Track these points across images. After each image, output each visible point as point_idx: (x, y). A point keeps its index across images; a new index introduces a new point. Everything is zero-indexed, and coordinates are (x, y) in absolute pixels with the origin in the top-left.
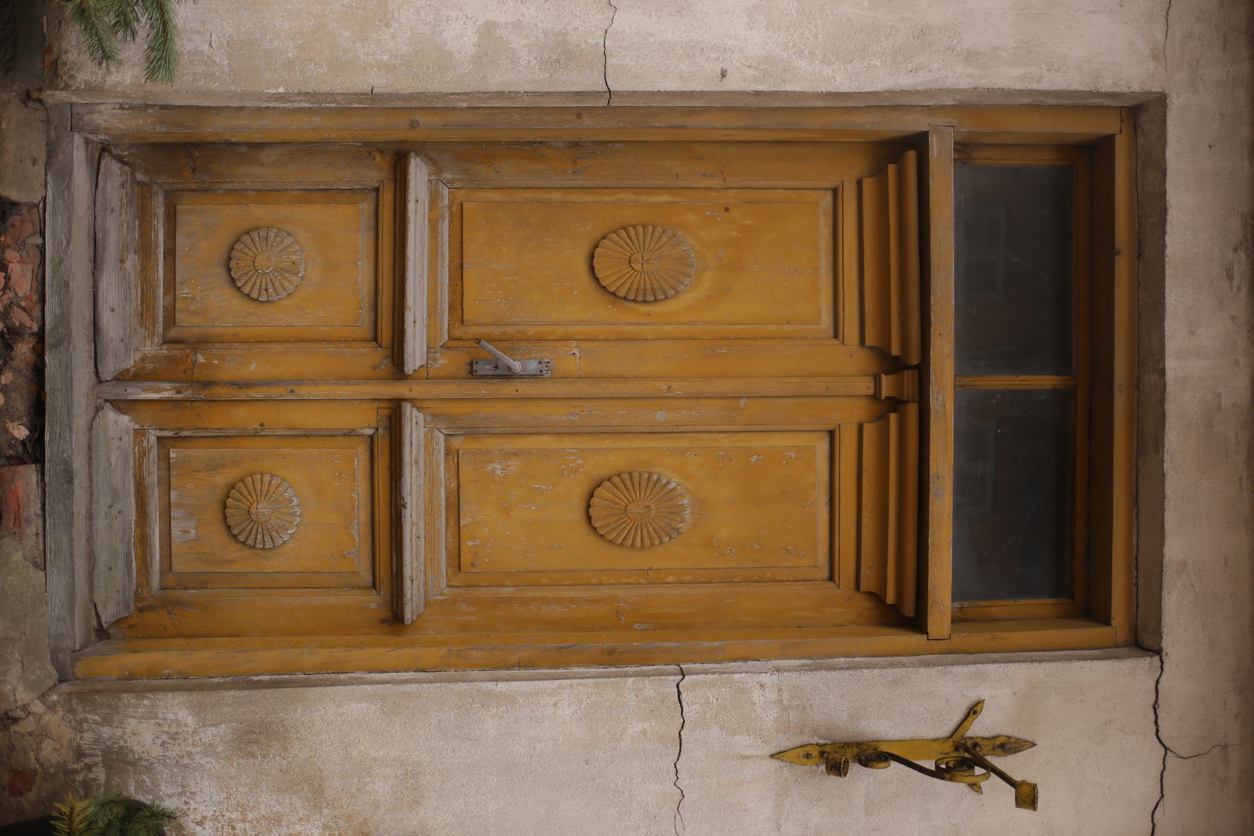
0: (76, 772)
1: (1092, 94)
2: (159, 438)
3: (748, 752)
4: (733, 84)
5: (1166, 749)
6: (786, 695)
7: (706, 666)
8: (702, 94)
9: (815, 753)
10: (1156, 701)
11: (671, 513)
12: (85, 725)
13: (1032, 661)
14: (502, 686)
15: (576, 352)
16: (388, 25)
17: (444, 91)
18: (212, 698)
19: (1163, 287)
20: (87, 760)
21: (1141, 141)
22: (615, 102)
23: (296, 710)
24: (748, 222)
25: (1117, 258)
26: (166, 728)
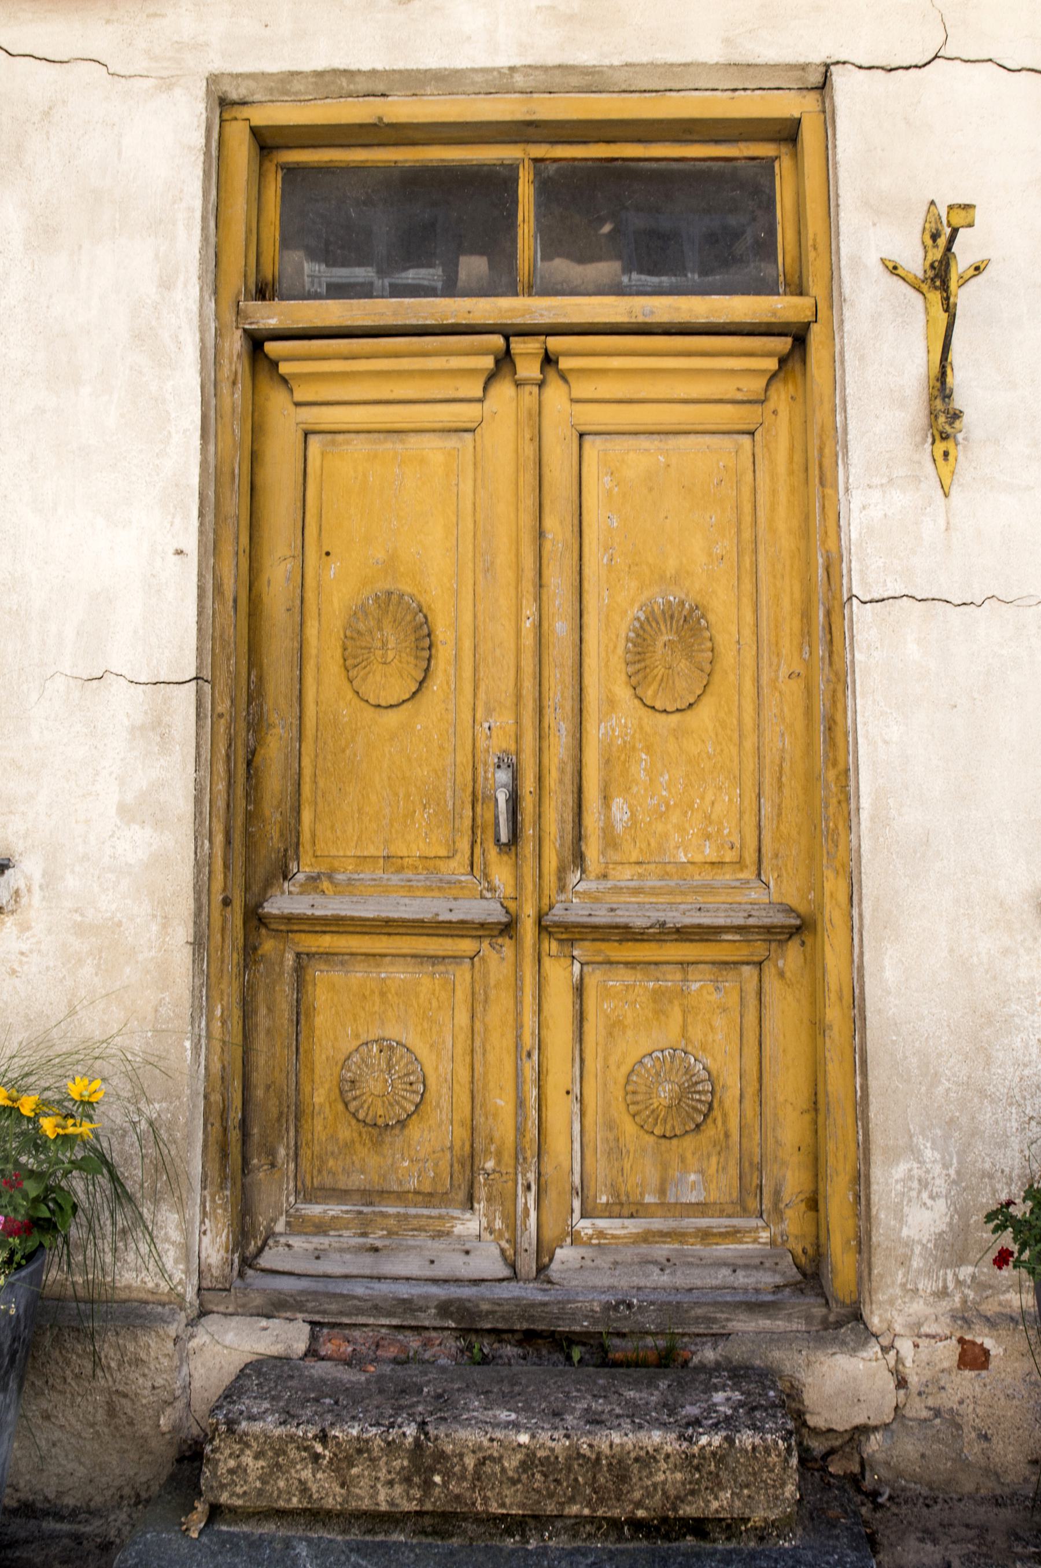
0: (964, 1301)
1: (207, 153)
2: (582, 1217)
3: (942, 523)
4: (191, 542)
5: (936, 57)
6: (876, 481)
7: (845, 572)
8: (201, 575)
9: (941, 447)
10: (882, 68)
11: (672, 617)
12: (909, 1287)
13: (838, 205)
14: (865, 802)
15: (486, 725)
16: (120, 924)
17: (192, 862)
18: (878, 1139)
19: (418, 71)
20: (951, 1285)
21: (257, 97)
22: (207, 674)
23: (894, 1042)
24: (632, 1393)
25: (386, 120)
26: (914, 1194)
